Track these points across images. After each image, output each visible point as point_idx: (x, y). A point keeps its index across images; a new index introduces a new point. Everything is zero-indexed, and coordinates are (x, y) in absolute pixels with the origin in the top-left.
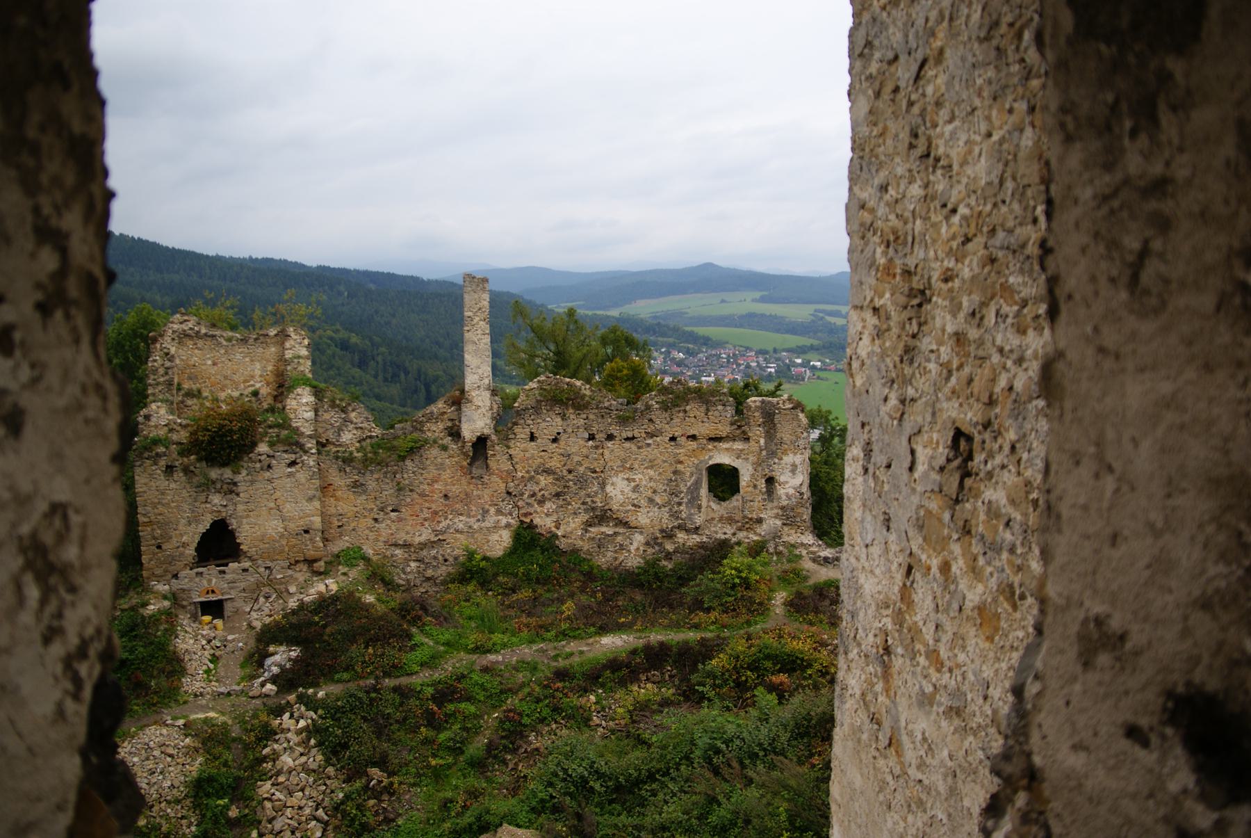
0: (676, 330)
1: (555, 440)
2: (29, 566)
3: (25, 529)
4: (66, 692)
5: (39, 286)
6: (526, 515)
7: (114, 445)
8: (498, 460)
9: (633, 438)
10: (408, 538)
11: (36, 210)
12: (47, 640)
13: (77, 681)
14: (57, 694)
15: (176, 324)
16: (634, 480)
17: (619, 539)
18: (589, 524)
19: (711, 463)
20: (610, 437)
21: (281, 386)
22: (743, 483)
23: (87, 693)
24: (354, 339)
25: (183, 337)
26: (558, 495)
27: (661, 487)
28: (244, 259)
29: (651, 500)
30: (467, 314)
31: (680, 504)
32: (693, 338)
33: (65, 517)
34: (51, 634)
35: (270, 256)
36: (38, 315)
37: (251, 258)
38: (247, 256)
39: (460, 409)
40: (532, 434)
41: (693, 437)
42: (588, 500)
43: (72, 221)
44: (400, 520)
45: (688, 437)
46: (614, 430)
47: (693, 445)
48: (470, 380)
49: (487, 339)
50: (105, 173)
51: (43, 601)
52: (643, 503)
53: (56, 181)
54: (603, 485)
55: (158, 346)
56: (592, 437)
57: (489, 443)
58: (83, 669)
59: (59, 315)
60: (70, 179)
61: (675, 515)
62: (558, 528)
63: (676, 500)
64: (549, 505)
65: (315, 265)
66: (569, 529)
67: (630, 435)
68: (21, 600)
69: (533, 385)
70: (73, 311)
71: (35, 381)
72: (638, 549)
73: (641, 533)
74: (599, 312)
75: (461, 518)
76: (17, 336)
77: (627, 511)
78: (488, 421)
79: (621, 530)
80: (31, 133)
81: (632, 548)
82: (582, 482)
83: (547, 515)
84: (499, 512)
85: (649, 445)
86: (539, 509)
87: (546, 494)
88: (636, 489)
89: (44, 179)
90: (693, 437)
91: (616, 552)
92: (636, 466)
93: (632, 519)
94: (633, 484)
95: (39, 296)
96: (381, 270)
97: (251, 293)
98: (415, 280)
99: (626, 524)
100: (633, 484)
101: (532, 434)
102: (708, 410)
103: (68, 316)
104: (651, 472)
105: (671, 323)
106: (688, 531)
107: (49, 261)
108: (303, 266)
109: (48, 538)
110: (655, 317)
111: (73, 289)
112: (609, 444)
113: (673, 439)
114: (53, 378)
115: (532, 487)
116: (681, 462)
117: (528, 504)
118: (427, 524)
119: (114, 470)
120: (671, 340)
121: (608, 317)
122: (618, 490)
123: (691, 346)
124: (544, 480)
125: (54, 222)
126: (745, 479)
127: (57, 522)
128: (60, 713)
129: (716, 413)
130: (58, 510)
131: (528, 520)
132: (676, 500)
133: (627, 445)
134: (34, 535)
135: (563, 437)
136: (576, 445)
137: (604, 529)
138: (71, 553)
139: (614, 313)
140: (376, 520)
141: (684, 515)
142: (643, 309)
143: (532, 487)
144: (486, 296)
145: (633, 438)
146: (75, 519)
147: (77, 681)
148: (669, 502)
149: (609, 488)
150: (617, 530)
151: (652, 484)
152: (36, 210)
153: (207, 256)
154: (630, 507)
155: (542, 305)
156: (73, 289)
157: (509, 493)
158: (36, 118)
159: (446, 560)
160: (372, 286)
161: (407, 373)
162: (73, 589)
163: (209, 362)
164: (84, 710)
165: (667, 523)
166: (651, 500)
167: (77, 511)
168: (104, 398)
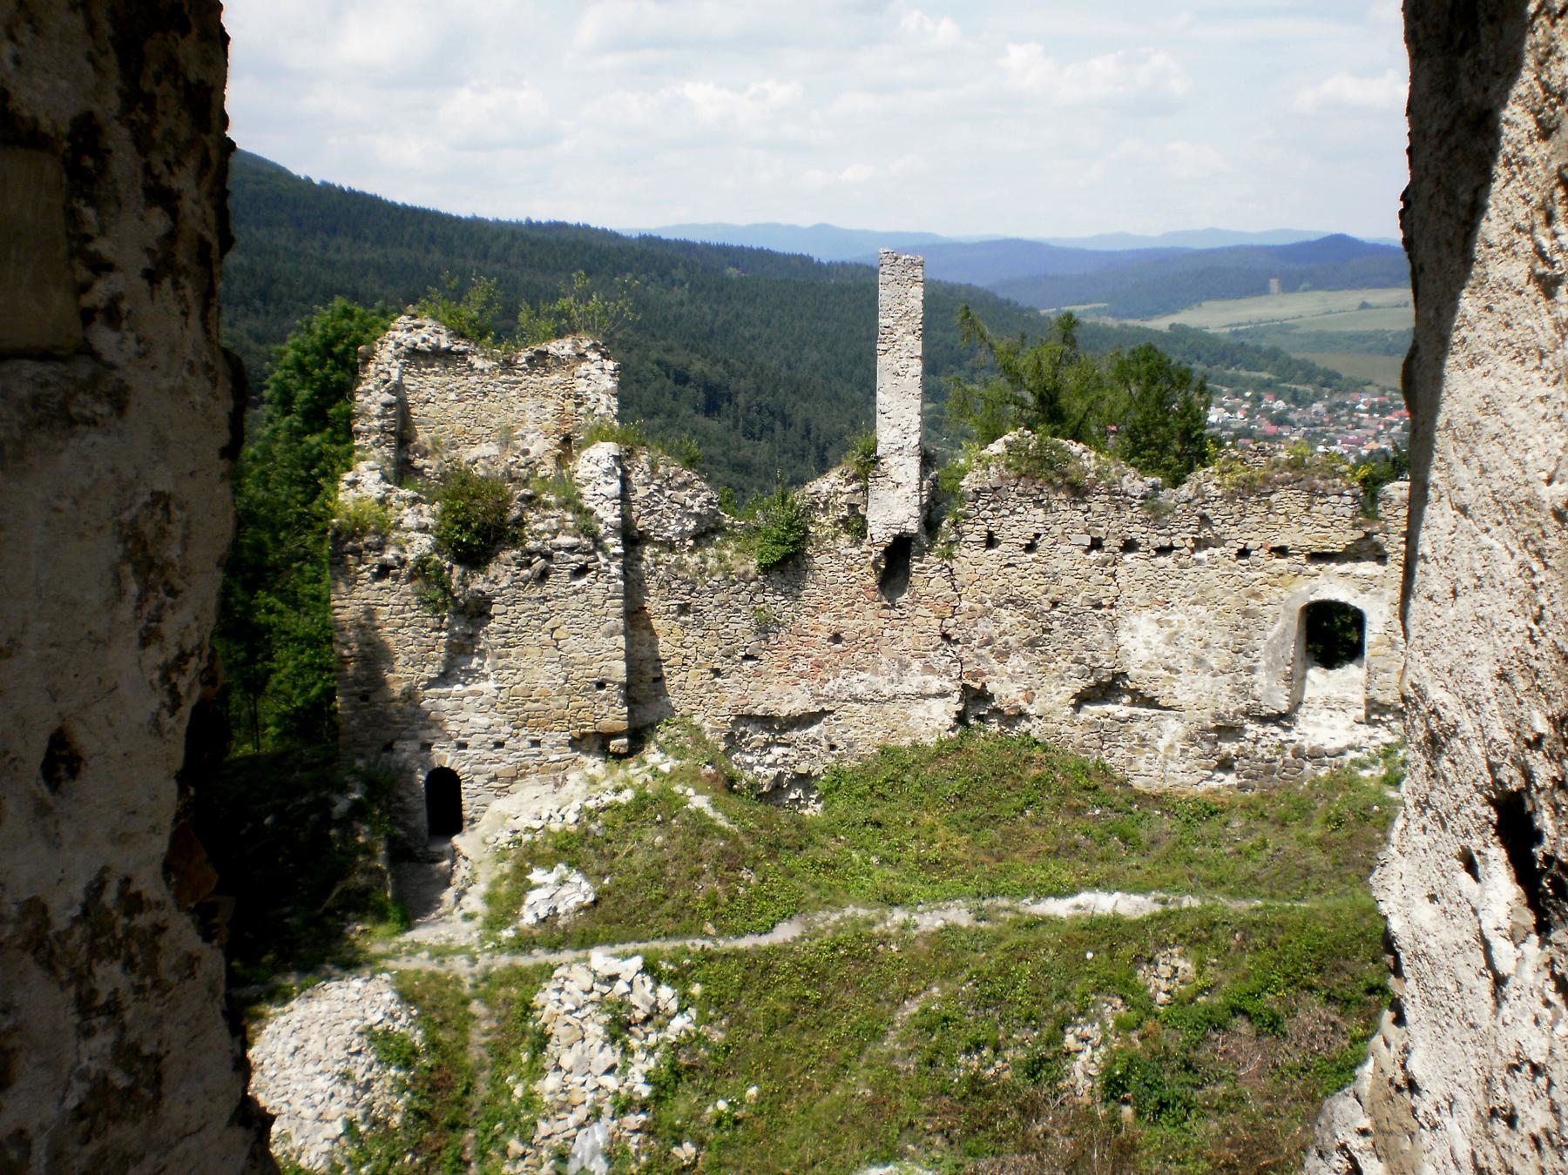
0: (1274, 354)
1: (1030, 548)
2: (127, 557)
3: (126, 516)
4: (163, 705)
5: (148, 251)
6: (975, 676)
7: (224, 438)
8: (926, 573)
9: (1171, 548)
10: (771, 706)
11: (148, 169)
12: (145, 642)
13: (173, 691)
14: (153, 705)
15: (413, 330)
16: (1169, 624)
17: (1139, 727)
18: (1082, 699)
19: (1313, 598)
20: (1129, 546)
21: (567, 440)
22: (1370, 638)
23: (186, 711)
24: (698, 366)
25: (415, 356)
26: (1032, 643)
27: (1218, 638)
28: (519, 224)
29: (1199, 662)
30: (883, 322)
31: (1251, 670)
32: (1309, 373)
33: (166, 508)
34: (148, 638)
35: (560, 219)
36: (145, 284)
37: (529, 222)
38: (523, 219)
39: (865, 489)
40: (990, 534)
41: (1282, 551)
42: (1087, 655)
43: (184, 181)
44: (758, 674)
45: (1273, 550)
46: (1136, 532)
47: (1283, 563)
48: (886, 435)
49: (917, 367)
50: (225, 121)
51: (142, 599)
52: (1186, 664)
53: (170, 135)
54: (1113, 630)
55: (371, 367)
56: (1096, 544)
57: (915, 548)
58: (183, 684)
59: (167, 283)
60: (184, 132)
61: (1242, 691)
62: (1030, 703)
63: (1245, 662)
64: (1016, 662)
65: (635, 235)
66: (1049, 705)
67: (1165, 542)
68: (121, 594)
69: (997, 447)
70: (182, 280)
71: (142, 355)
72: (1171, 746)
73: (1179, 718)
74: (1131, 322)
75: (863, 676)
76: (124, 306)
77: (1155, 679)
78: (916, 511)
79: (1142, 711)
80: (147, 85)
81: (1161, 745)
82: (1077, 626)
83: (1012, 678)
84: (928, 668)
85: (1199, 562)
86: (998, 668)
87: (1012, 640)
88: (1172, 640)
89: (157, 134)
90: (1282, 551)
91: (1131, 749)
92: (1175, 599)
93: (1163, 694)
94: (1167, 630)
95: (146, 262)
96: (747, 244)
97: (508, 281)
98: (805, 261)
99: (1151, 703)
100: (1167, 630)
101: (990, 534)
102: (1311, 502)
103: (176, 285)
104: (1201, 610)
105: (1265, 344)
106: (1264, 720)
107: (158, 222)
108: (615, 236)
109: (148, 529)
110: (1237, 333)
111: (182, 257)
112: (1128, 557)
113: (1244, 553)
114: (160, 355)
115: (985, 628)
116: (1256, 595)
117: (979, 657)
118: (803, 683)
119: (223, 465)
120: (1265, 375)
121: (1149, 331)
122: (1140, 643)
123: (1300, 388)
124: (1009, 618)
125: (164, 182)
126: (1374, 632)
127: (159, 515)
128: (156, 723)
129: (1326, 509)
130: (160, 500)
131: (977, 686)
132: (1245, 662)
133: (1161, 560)
134: (133, 524)
135: (1043, 545)
136: (1068, 557)
137: (1110, 708)
138: (173, 552)
139: (1162, 324)
140: (717, 672)
141: (1258, 691)
142: (1214, 318)
143: (985, 628)
144: (918, 291)
145: (1171, 548)
146: (177, 514)
147: (173, 691)
148: (1231, 668)
149: (1123, 636)
150: (1135, 710)
151: (1202, 632)
152: (148, 169)
153: (458, 219)
154: (1161, 672)
155: (1031, 309)
156: (182, 257)
157: (946, 637)
158: (152, 68)
159: (833, 747)
160: (732, 272)
161: (787, 423)
162: (172, 592)
163: (452, 396)
164: (182, 729)
165: (1229, 705)
166: (1199, 662)
167: (181, 508)
168: (214, 381)
